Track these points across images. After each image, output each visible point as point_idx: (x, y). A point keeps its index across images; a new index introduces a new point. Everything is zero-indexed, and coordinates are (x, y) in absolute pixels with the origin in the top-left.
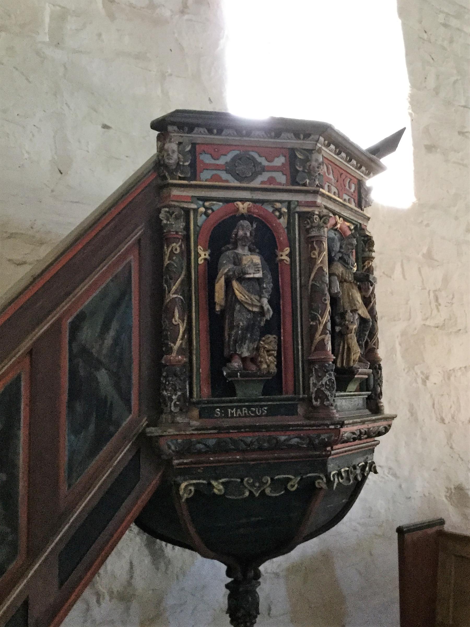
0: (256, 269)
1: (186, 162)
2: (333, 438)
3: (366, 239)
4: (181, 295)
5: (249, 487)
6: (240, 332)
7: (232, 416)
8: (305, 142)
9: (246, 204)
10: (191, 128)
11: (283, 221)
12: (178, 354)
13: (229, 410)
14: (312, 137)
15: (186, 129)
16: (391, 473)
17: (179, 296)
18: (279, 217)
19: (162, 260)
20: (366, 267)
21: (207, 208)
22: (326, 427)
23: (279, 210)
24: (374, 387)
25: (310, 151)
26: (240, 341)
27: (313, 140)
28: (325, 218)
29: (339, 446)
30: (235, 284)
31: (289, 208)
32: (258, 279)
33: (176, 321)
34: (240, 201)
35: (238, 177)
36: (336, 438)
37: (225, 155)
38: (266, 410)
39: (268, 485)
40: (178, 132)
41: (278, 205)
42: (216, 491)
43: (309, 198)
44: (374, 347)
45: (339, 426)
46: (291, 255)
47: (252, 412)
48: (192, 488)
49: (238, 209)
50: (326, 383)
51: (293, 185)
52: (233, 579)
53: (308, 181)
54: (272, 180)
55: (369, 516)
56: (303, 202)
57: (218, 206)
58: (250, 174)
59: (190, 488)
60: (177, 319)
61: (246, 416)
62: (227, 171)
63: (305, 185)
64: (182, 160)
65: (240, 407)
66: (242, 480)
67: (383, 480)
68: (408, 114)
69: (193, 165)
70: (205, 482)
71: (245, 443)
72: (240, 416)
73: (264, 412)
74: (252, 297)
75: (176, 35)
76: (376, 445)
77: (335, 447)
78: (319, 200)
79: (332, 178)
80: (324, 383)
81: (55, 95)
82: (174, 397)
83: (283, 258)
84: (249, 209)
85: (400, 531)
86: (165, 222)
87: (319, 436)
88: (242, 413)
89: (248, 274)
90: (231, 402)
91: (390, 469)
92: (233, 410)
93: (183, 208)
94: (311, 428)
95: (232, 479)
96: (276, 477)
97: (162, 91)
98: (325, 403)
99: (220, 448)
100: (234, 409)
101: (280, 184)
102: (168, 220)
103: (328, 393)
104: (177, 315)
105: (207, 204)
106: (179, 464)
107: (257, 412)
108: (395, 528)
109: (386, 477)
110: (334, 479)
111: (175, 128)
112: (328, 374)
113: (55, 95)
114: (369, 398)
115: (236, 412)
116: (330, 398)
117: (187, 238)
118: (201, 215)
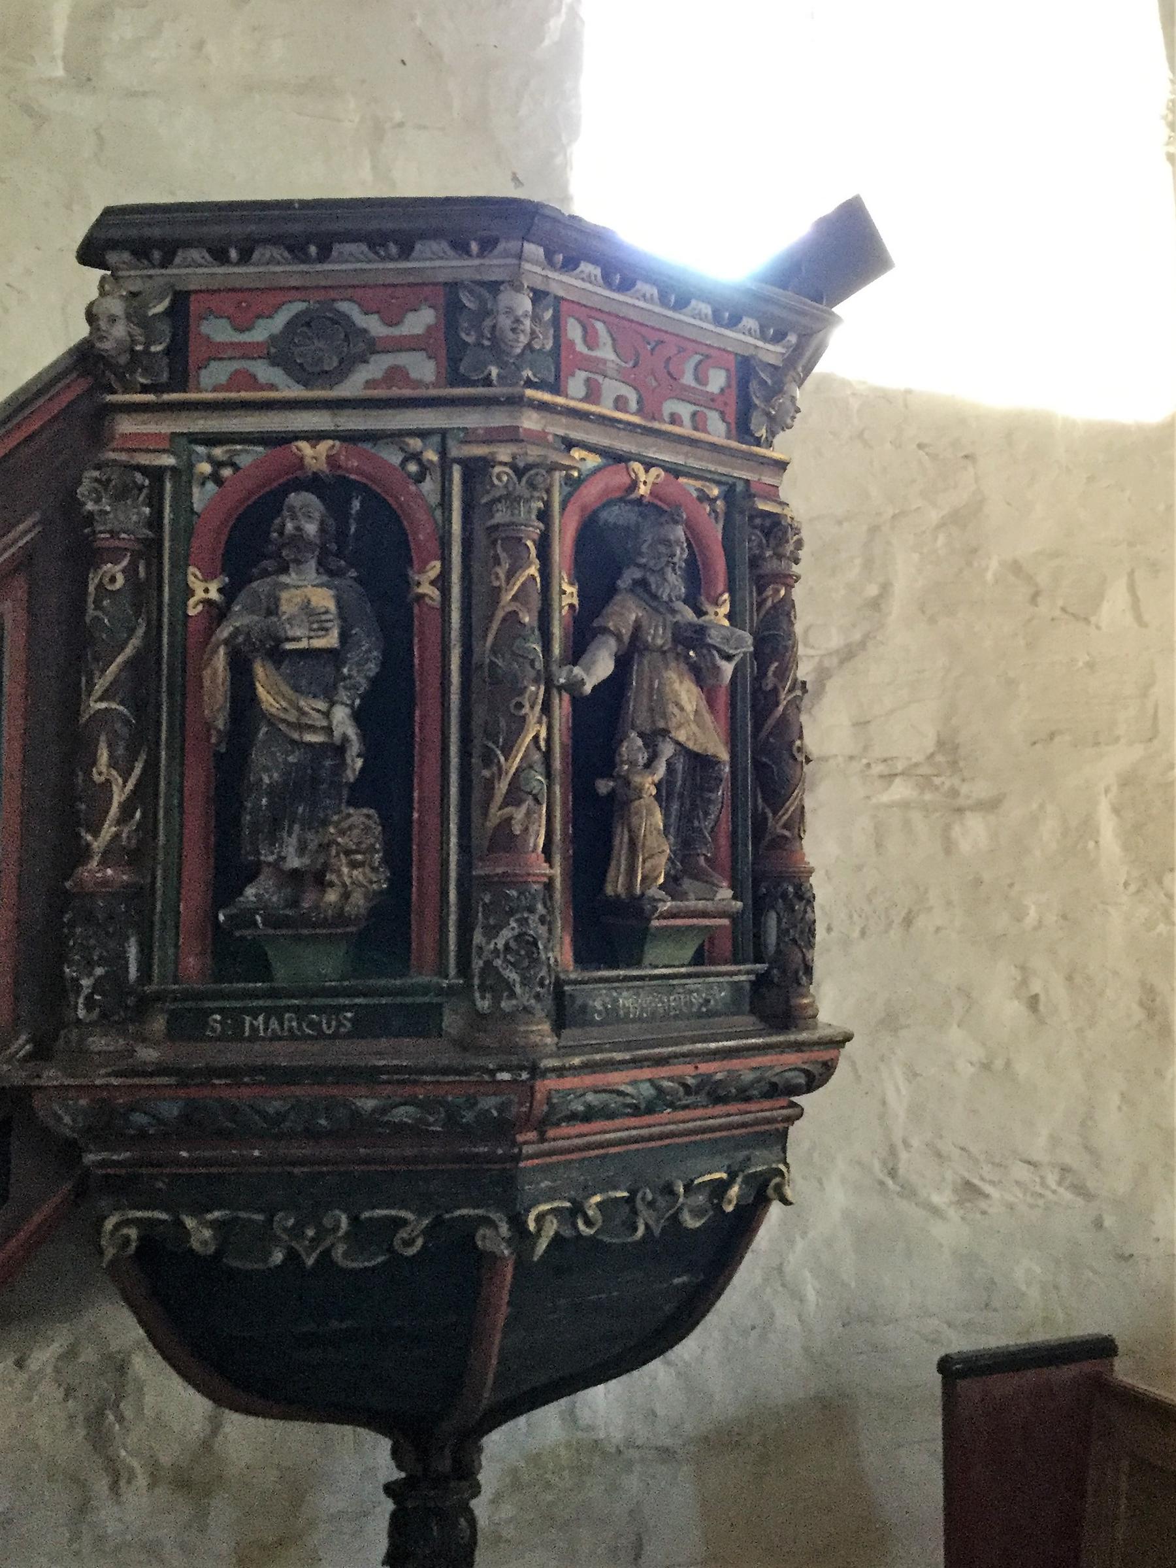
0: (315, 626)
1: (154, 343)
2: (514, 1109)
3: (768, 523)
4: (121, 703)
5: (285, 1237)
6: (264, 801)
7: (254, 1037)
8: (487, 262)
9: (324, 446)
10: (169, 251)
11: (429, 487)
12: (104, 863)
13: (248, 1019)
14: (501, 246)
15: (157, 255)
16: (1067, 1183)
17: (114, 706)
18: (419, 478)
19: (83, 611)
20: (769, 603)
21: (218, 465)
22: (486, 1078)
23: (416, 457)
24: (779, 952)
25: (494, 287)
26: (274, 827)
27: (506, 254)
28: (532, 472)
29: (565, 1129)
30: (260, 670)
31: (443, 452)
32: (330, 651)
33: (100, 774)
34: (418, 436)
35: (304, 377)
36: (524, 1109)
37: (270, 317)
38: (350, 1020)
39: (341, 1233)
40: (136, 268)
41: (415, 444)
42: (195, 1245)
43: (499, 419)
44: (787, 833)
45: (525, 1076)
46: (442, 582)
47: (311, 1025)
48: (133, 1233)
49: (302, 459)
50: (507, 947)
51: (452, 385)
52: (403, 1475)
53: (494, 371)
54: (395, 375)
55: (987, 1305)
56: (481, 432)
57: (248, 457)
58: (335, 364)
59: (125, 1231)
60: (104, 769)
61: (293, 1037)
62: (274, 361)
63: (487, 382)
64: (141, 339)
65: (278, 1013)
66: (270, 1220)
67: (1041, 1202)
68: (1164, 157)
69: (178, 351)
70: (163, 1216)
71: (264, 1115)
72: (276, 1038)
73: (344, 1026)
74: (302, 703)
75: (419, 22)
76: (791, 1120)
77: (551, 1133)
78: (530, 422)
79: (611, 356)
80: (500, 946)
81: (68, 207)
82: (84, 982)
83: (420, 590)
84: (331, 460)
85: (953, 1370)
86: (90, 506)
87: (472, 1103)
88: (282, 1029)
89: (288, 640)
90: (254, 995)
91: (1065, 1170)
92: (256, 1018)
93: (144, 470)
94: (442, 1079)
95: (243, 1215)
96: (366, 1214)
97: (374, 168)
98: (503, 1004)
99: (193, 1124)
100: (261, 1018)
101: (418, 384)
102: (97, 501)
103: (513, 976)
104: (104, 756)
105: (218, 452)
106: (102, 1164)
107: (324, 1026)
108: (936, 1359)
109: (1048, 1193)
110: (539, 1230)
111: (126, 256)
112: (517, 921)
113: (68, 207)
114: (761, 982)
115: (266, 1023)
116: (518, 990)
117: (151, 549)
118: (203, 484)
